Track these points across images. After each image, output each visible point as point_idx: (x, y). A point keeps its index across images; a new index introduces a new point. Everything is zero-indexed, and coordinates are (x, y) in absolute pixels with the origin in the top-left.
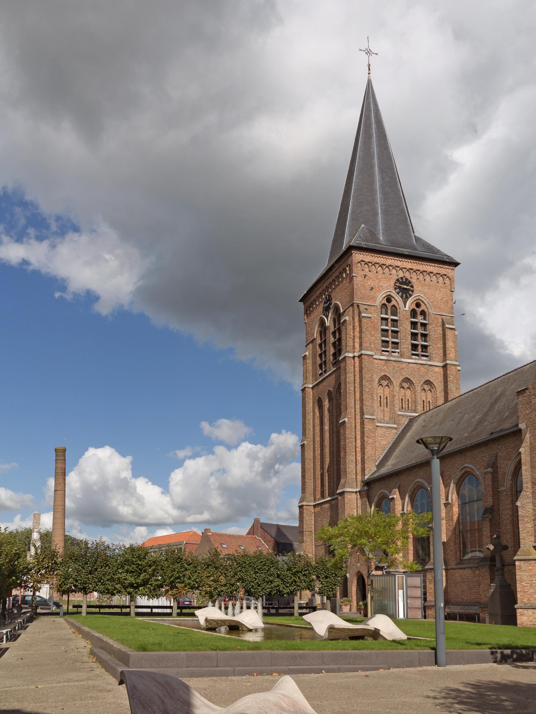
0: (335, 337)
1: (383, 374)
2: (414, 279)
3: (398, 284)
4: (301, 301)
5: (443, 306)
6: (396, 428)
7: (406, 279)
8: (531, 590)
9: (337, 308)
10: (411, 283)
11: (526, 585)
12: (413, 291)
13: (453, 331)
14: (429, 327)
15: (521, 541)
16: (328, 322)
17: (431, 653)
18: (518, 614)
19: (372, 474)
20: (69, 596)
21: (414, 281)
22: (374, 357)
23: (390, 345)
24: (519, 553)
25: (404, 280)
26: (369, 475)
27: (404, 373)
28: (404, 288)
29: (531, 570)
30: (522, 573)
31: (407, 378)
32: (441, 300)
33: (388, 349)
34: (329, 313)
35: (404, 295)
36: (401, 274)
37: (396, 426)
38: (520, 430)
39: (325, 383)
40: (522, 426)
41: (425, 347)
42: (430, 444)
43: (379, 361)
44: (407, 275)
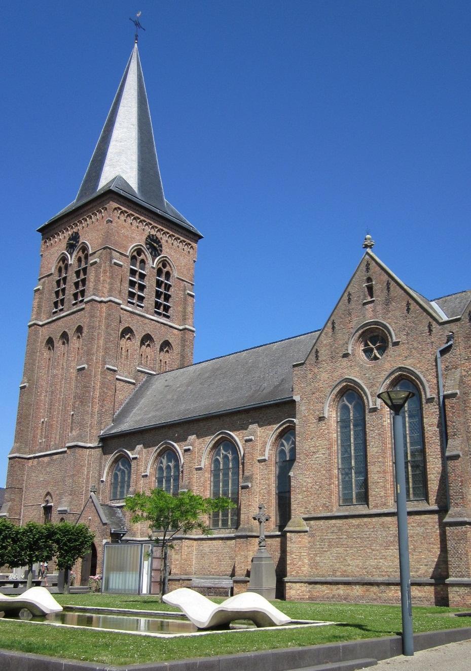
0: (78, 276)
1: (127, 326)
2: (164, 239)
3: (149, 240)
4: (39, 231)
5: (185, 272)
6: (134, 384)
7: (157, 238)
8: (300, 563)
9: (84, 249)
10: (160, 242)
11: (295, 557)
12: (161, 251)
13: (192, 298)
14: (172, 289)
15: (292, 511)
16: (72, 260)
17: (398, 639)
18: (287, 588)
19: (109, 429)
20: (430, 584)
21: (163, 242)
22: (122, 306)
23: (136, 297)
24: (289, 523)
25: (155, 238)
26: (105, 430)
27: (146, 329)
28: (154, 245)
29: (300, 542)
30: (293, 545)
31: (148, 334)
32: (185, 266)
33: (134, 301)
34: (73, 251)
35: (153, 253)
36: (153, 232)
37: (134, 381)
38: (294, 401)
39: (60, 323)
40: (297, 398)
41: (167, 308)
42: (394, 399)
43: (125, 312)
44: (159, 235)
